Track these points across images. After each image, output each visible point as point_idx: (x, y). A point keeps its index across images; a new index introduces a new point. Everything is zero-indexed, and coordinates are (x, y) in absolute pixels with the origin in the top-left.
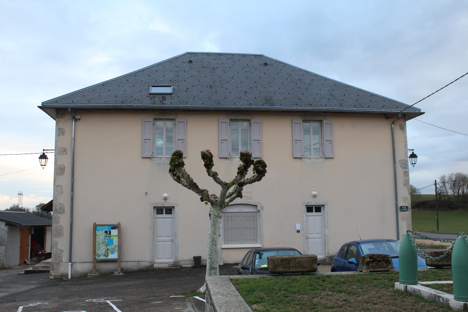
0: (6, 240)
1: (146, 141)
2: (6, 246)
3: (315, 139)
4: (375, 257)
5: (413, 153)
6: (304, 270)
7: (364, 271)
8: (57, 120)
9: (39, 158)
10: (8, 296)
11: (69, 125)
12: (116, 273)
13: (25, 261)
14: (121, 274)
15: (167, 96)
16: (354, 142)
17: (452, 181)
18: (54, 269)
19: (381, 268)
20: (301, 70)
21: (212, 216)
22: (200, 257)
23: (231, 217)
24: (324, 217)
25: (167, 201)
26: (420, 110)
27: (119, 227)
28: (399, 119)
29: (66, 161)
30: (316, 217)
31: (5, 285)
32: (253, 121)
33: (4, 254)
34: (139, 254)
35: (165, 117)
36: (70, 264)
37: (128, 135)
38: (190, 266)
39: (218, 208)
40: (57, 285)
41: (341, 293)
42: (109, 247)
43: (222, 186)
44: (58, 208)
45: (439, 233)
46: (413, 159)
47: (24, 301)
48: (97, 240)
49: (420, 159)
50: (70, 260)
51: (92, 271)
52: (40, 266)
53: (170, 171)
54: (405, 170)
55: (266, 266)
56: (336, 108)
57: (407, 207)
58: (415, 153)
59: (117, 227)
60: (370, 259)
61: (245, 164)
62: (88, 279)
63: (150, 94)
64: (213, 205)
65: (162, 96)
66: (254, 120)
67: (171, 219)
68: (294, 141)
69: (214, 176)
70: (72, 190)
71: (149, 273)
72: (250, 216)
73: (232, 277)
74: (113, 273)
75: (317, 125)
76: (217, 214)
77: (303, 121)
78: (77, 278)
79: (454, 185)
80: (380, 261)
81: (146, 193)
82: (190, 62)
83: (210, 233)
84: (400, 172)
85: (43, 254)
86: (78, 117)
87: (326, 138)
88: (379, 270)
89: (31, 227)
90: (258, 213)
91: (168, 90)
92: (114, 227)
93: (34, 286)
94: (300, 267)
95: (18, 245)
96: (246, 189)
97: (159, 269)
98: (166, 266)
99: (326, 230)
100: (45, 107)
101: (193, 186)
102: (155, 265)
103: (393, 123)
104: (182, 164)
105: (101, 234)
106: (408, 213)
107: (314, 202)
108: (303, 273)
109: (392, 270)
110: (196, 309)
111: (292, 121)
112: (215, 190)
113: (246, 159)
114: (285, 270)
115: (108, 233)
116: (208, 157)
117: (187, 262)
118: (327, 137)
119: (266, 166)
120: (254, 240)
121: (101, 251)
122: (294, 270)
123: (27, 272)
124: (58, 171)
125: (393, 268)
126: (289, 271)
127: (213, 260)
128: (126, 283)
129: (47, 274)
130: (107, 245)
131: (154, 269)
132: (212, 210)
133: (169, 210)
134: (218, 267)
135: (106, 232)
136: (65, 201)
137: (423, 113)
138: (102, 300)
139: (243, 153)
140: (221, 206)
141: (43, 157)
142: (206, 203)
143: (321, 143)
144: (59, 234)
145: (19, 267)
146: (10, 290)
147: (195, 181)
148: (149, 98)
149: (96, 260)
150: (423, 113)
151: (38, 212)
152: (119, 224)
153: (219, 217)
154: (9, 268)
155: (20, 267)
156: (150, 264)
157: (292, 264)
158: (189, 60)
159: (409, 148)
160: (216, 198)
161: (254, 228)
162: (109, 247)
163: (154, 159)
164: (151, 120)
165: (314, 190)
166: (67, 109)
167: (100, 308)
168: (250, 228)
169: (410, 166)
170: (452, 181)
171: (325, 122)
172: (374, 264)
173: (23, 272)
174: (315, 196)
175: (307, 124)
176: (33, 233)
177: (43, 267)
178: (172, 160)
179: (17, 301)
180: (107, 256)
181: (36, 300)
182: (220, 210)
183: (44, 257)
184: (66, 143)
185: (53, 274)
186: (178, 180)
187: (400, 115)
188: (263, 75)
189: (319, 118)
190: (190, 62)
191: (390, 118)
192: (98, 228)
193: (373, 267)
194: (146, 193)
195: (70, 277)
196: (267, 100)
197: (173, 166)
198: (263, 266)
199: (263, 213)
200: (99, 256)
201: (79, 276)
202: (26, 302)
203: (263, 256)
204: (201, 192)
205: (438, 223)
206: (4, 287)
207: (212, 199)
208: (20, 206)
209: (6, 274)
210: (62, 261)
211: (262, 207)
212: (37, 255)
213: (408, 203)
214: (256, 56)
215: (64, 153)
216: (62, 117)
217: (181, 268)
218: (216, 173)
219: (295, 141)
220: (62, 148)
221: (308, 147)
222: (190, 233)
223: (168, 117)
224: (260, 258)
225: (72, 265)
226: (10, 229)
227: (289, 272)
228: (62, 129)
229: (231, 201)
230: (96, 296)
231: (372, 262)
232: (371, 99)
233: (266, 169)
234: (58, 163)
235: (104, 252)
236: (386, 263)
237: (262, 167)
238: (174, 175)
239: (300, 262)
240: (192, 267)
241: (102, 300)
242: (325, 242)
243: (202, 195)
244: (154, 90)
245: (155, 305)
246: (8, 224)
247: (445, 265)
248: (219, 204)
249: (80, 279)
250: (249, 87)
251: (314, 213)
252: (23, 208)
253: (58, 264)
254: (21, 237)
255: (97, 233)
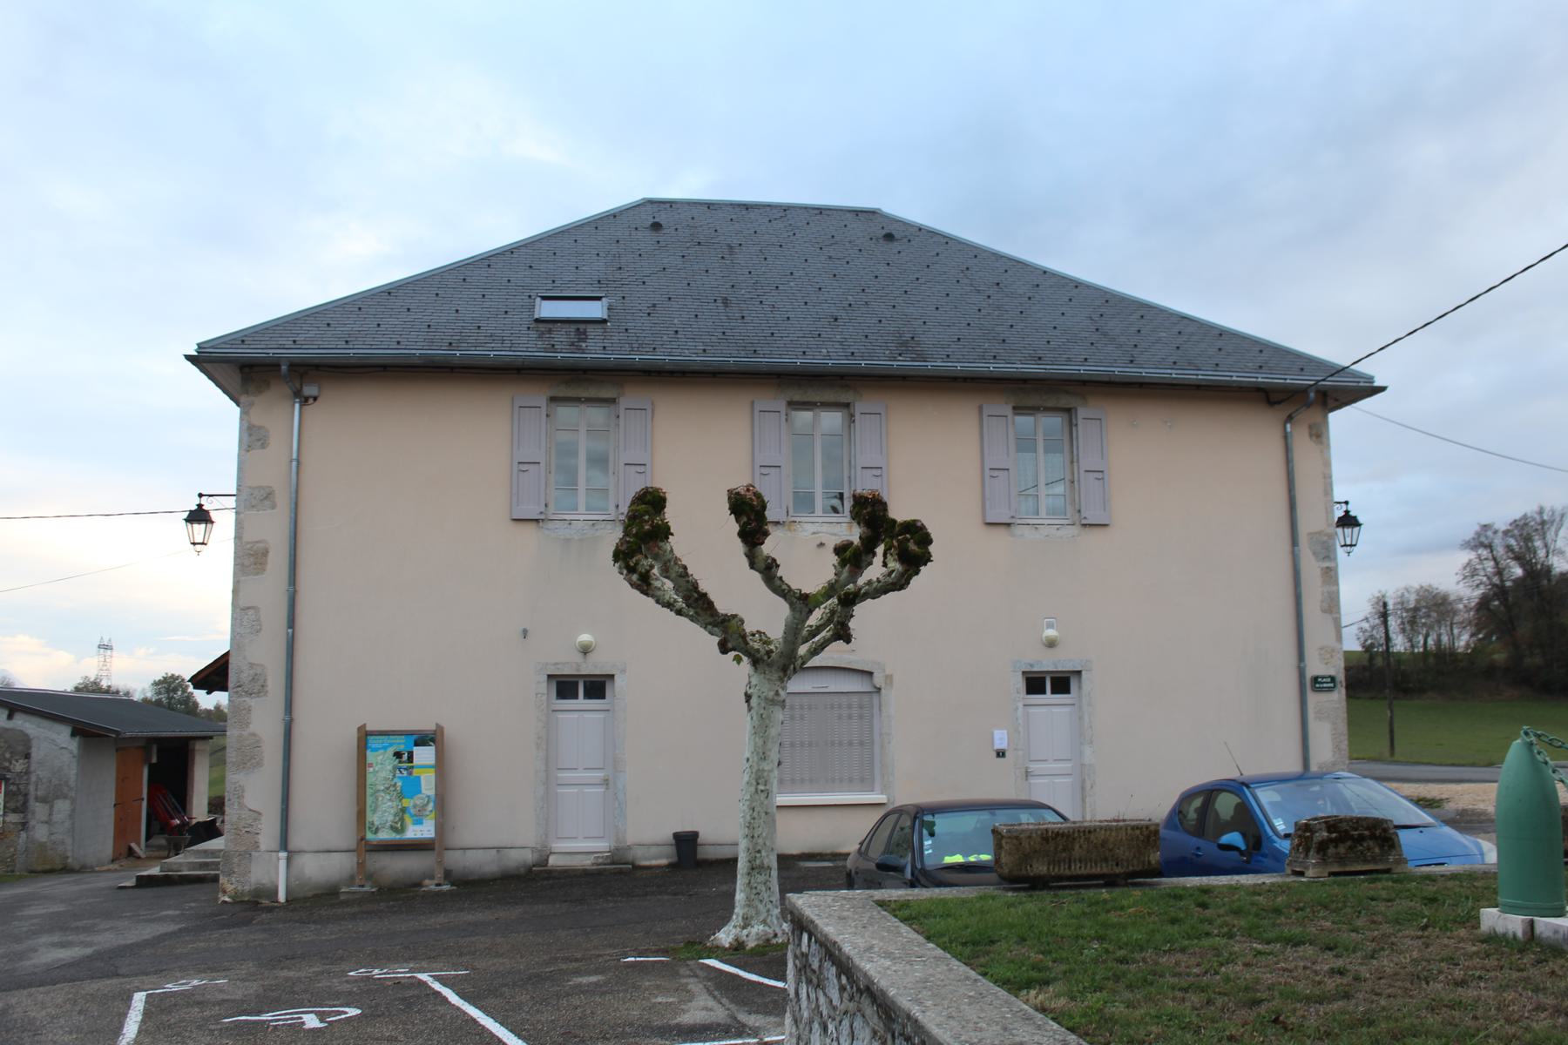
0: (72, 783)
1: (525, 467)
2: (73, 801)
3: (1048, 464)
4: (1344, 826)
5: (1347, 512)
6: (1118, 870)
7: (1310, 873)
8: (243, 399)
9: (187, 520)
10: (90, 958)
11: (283, 416)
12: (430, 885)
13: (130, 849)
14: (446, 888)
15: (590, 328)
16: (1174, 479)
17: (1407, 611)
18: (230, 873)
19: (1366, 861)
20: (997, 256)
21: (754, 701)
22: (695, 835)
23: (802, 707)
24: (1080, 708)
25: (592, 657)
26: (1370, 379)
27: (438, 738)
28: (1309, 405)
29: (272, 528)
30: (1055, 709)
31: (79, 924)
32: (860, 407)
33: (67, 824)
34: (503, 822)
35: (584, 394)
36: (283, 855)
37: (469, 448)
38: (664, 862)
39: (775, 676)
40: (247, 922)
41: (1297, 945)
42: (406, 803)
43: (791, 605)
44: (246, 676)
45: (1396, 763)
46: (1348, 531)
47: (147, 974)
48: (370, 779)
49: (1364, 535)
50: (284, 844)
51: (352, 878)
52: (185, 861)
53: (618, 555)
54: (1327, 564)
55: (985, 857)
56: (1119, 370)
57: (1333, 679)
58: (1352, 514)
59: (433, 740)
60: (1329, 831)
61: (869, 532)
62: (346, 903)
63: (538, 321)
64: (760, 666)
65: (573, 327)
66: (865, 404)
67: (601, 715)
68: (987, 473)
69: (768, 571)
70: (292, 622)
71: (533, 885)
72: (840, 706)
73: (879, 894)
74: (419, 885)
75: (1055, 421)
76: (772, 694)
77: (1014, 408)
78: (306, 899)
79: (1413, 621)
80: (1361, 839)
81: (525, 632)
82: (656, 226)
83: (747, 755)
84: (1311, 568)
85: (184, 824)
86: (309, 390)
87: (1085, 464)
88: (1365, 867)
89: (151, 741)
90: (875, 697)
91: (594, 310)
92: (423, 740)
93: (172, 927)
94: (1106, 860)
95: (110, 797)
96: (864, 615)
97: (566, 871)
98: (587, 862)
99: (1087, 751)
100: (207, 359)
101: (697, 605)
102: (552, 861)
103: (1290, 418)
104: (664, 532)
105: (381, 762)
106: (1338, 697)
107: (1047, 663)
108: (1110, 881)
109: (1399, 869)
110: (724, 1000)
111: (980, 409)
112: (766, 616)
113: (870, 511)
114: (1055, 871)
115: (405, 757)
116: (752, 506)
117: (654, 850)
118: (1088, 460)
119: (930, 542)
120: (862, 780)
121: (382, 814)
122: (1083, 871)
123: (144, 882)
124: (247, 562)
125: (1401, 861)
126: (1067, 872)
127: (760, 841)
128: (469, 917)
129: (207, 887)
130: (401, 796)
131: (550, 872)
132: (754, 681)
133: (597, 687)
134: (775, 865)
135: (398, 755)
136: (266, 655)
137: (1382, 389)
138: (402, 973)
139: (861, 497)
140: (784, 669)
141: (199, 516)
142: (738, 660)
143: (1068, 477)
144: (251, 760)
145: (111, 866)
146: (97, 938)
147: (703, 587)
148: (533, 334)
149: (367, 843)
150: (1382, 389)
151: (158, 703)
152: (440, 730)
153: (776, 702)
154: (83, 869)
155: (115, 866)
156: (536, 856)
157: (1077, 852)
158: (651, 221)
159: (1339, 495)
160: (767, 642)
161: (861, 744)
162: (406, 803)
163: (550, 525)
164: (542, 400)
165: (1050, 626)
166: (278, 366)
167: (404, 999)
168: (850, 744)
169: (1341, 552)
170: (1407, 611)
171: (1082, 413)
172: (1342, 849)
173: (131, 883)
174: (1051, 644)
175: (1025, 421)
176: (154, 760)
177: (193, 866)
178: (633, 518)
179: (124, 976)
180: (401, 830)
181: (185, 972)
182: (781, 680)
183: (188, 836)
184: (273, 473)
185: (230, 888)
186: (644, 584)
187: (1312, 395)
188: (883, 268)
189: (1064, 401)
190: (656, 226)
191: (1279, 403)
192: (373, 742)
193: (1341, 860)
194: (525, 632)
195: (282, 897)
196: (904, 344)
197: (636, 535)
198: (949, 860)
199: (891, 697)
200: (376, 832)
201: (310, 894)
202: (153, 978)
203: (936, 829)
204: (723, 621)
205: (1392, 731)
206: (77, 930)
207: (756, 645)
208: (104, 684)
209: (76, 888)
210: (256, 846)
211: (889, 678)
212: (166, 829)
213: (1336, 668)
214: (857, 213)
215: (267, 503)
216: (259, 391)
217: (636, 868)
218: (774, 560)
219: (990, 472)
220: (260, 488)
221: (1030, 492)
222: (673, 753)
223: (592, 392)
224: (932, 834)
225: (289, 860)
226: (85, 750)
227: (1070, 878)
228: (260, 428)
229: (815, 652)
230: (377, 959)
231: (1336, 842)
232: (1220, 344)
233: (931, 548)
234: (247, 537)
235: (391, 818)
236: (1382, 847)
237: (917, 543)
238: (631, 570)
239: (1104, 843)
240: (670, 866)
241: (402, 973)
242: (1083, 788)
243: (725, 631)
244: (548, 310)
245: (581, 990)
246: (82, 731)
247: (1060, 878)
248: (776, 663)
249: (316, 902)
250: (846, 304)
251: (1049, 697)
252: (113, 689)
253: (247, 855)
254: (118, 771)
255: (371, 757)
